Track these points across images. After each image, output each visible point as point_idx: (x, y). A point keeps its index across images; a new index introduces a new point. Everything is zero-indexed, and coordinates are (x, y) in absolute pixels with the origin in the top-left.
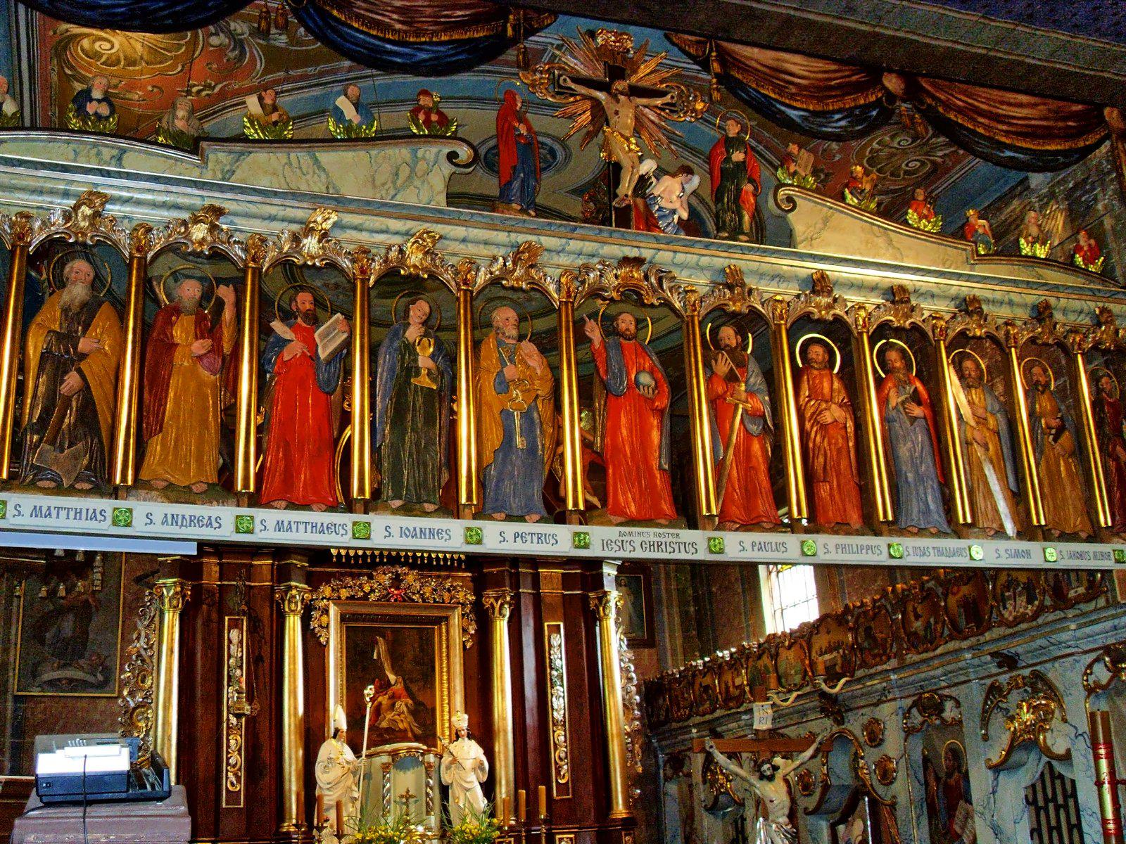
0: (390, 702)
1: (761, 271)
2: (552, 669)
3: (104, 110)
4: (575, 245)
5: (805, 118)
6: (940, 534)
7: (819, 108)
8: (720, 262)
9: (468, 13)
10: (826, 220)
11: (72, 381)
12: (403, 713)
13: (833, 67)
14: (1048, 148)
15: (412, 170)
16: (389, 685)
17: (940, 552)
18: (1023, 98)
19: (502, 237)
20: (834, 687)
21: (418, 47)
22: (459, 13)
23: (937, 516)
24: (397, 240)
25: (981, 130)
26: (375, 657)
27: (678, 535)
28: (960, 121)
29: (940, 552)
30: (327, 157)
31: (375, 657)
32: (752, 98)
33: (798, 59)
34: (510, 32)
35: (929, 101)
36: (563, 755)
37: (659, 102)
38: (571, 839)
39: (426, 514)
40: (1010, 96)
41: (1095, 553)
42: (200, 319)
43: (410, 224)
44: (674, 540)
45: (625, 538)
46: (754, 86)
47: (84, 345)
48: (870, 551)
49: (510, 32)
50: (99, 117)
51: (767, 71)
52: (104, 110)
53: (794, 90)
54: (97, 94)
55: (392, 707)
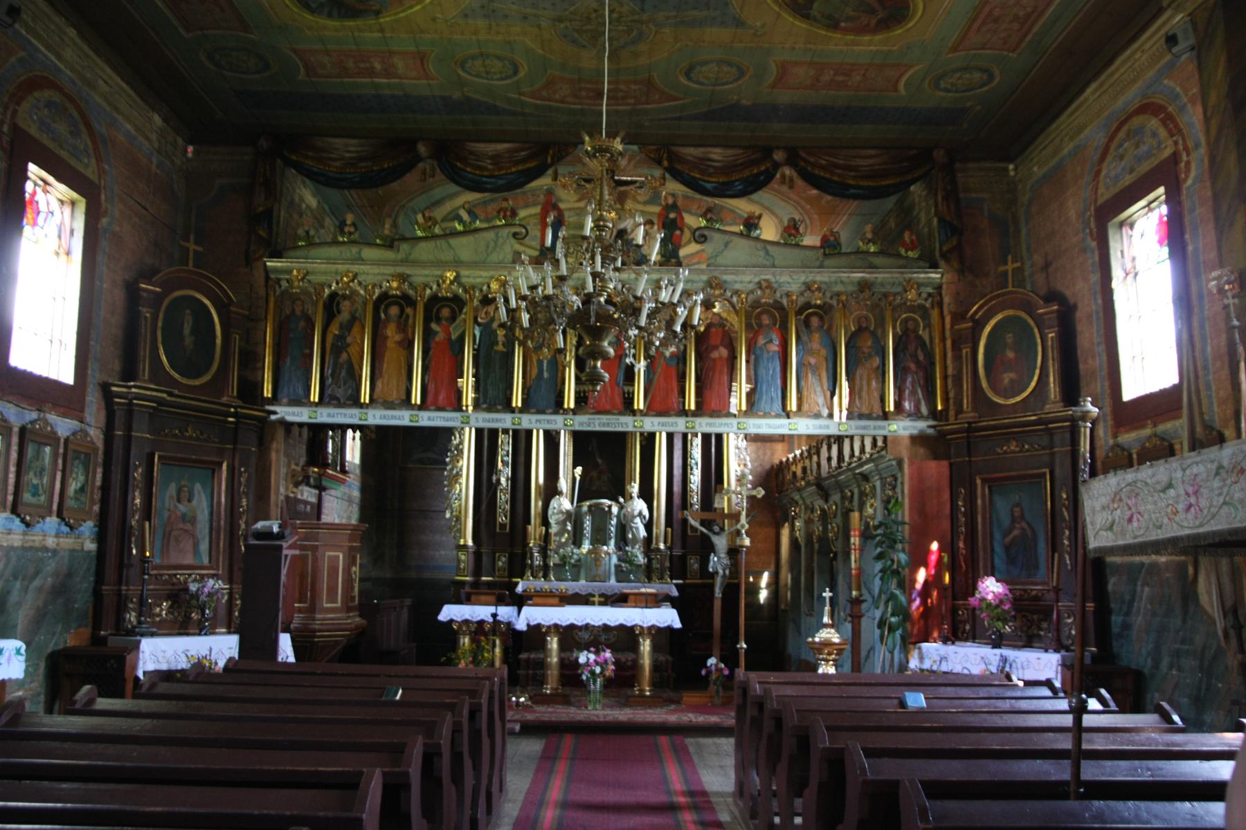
3: (352, 229)
5: (715, 188)
6: (778, 416)
10: (726, 245)
11: (344, 356)
14: (883, 183)
18: (872, 152)
20: (336, 602)
23: (777, 405)
25: (836, 178)
30: (454, 241)
33: (718, 150)
34: (549, 160)
35: (802, 164)
39: (498, 411)
43: (492, 273)
47: (349, 340)
49: (549, 160)
52: (352, 229)
53: (711, 170)
54: (349, 222)
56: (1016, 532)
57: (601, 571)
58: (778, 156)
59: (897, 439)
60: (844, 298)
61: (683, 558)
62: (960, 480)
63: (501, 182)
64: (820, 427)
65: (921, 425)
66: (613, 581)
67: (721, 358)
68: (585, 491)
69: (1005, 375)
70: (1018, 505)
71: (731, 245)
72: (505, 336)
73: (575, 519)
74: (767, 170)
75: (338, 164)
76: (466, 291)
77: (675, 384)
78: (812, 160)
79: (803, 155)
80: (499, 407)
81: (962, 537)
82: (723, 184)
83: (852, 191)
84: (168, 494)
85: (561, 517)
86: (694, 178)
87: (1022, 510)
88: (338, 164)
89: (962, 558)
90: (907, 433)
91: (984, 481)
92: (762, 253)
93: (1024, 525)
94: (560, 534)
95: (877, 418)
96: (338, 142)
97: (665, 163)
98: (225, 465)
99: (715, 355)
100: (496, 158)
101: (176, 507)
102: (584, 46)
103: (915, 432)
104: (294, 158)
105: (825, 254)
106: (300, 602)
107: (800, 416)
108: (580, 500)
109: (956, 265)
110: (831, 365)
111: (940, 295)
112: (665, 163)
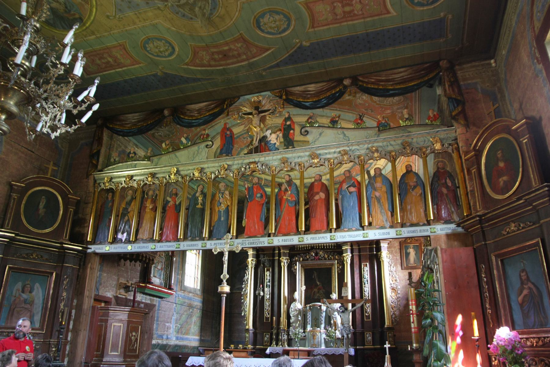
4: (236, 162)
6: (357, 230)
7: (317, 99)
8: (279, 157)
10: (320, 134)
13: (325, 84)
14: (410, 85)
15: (198, 152)
16: (317, 285)
17: (350, 236)
18: (402, 70)
19: (217, 165)
21: (200, 119)
23: (295, 229)
24: (192, 171)
25: (381, 87)
29: (350, 236)
33: (312, 85)
34: (225, 106)
35: (360, 83)
39: (196, 240)
40: (396, 71)
41: (340, 236)
42: (152, 199)
43: (194, 167)
49: (225, 106)
50: (132, 157)
52: (133, 155)
53: (309, 96)
54: (132, 152)
55: (318, 292)
56: (525, 292)
57: (316, 341)
58: (347, 82)
59: (437, 238)
60: (394, 154)
61: (363, 334)
62: (480, 258)
63: (201, 121)
64: (384, 234)
65: (451, 228)
66: (323, 347)
67: (321, 198)
68: (309, 299)
69: (500, 180)
70: (523, 270)
71: (323, 134)
72: (202, 200)
73: (303, 314)
74: (340, 90)
75: (129, 126)
76: (182, 178)
77: (294, 218)
78: (366, 80)
79: (361, 79)
80: (197, 238)
81: (488, 301)
82: (315, 102)
83: (391, 92)
84: (16, 288)
85: (296, 313)
86: (299, 101)
87: (527, 274)
88: (129, 126)
89: (490, 317)
90: (444, 232)
91: (497, 256)
92: (342, 136)
93: (530, 285)
94: (296, 322)
95: (424, 225)
96: (130, 116)
97: (284, 97)
98: (54, 274)
99: (317, 197)
100: (199, 111)
101: (20, 295)
102: (191, 18)
103: (449, 231)
104: (111, 126)
105: (379, 130)
106: (97, 351)
107: (371, 229)
108: (306, 303)
109: (462, 122)
110: (390, 197)
111: (457, 144)
112: (284, 97)
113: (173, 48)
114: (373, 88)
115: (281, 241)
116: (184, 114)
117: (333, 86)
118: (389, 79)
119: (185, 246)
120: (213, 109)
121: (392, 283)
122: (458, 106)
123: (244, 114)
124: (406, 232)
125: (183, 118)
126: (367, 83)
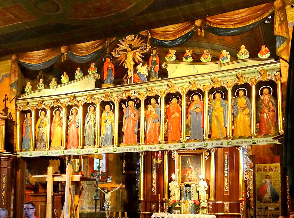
0: (191, 172)
1: (156, 85)
2: (225, 164)
9: (98, 44)
10: (177, 67)
12: (194, 175)
22: (97, 44)
25: (224, 27)
26: (188, 162)
27: (133, 147)
28: (217, 27)
31: (188, 162)
32: (158, 42)
35: (208, 24)
36: (227, 185)
37: (138, 50)
38: (211, 204)
41: (188, 145)
44: (132, 148)
45: (123, 149)
46: (158, 39)
48: (176, 147)
51: (162, 33)
74: (192, 30)
75: (36, 61)
99: (174, 116)
100: (87, 49)
113: (58, 7)
114: (218, 28)
115: (148, 148)
116: (76, 51)
117: (188, 26)
118: (231, 19)
119: (84, 151)
120: (97, 47)
121: (246, 167)
122: (283, 43)
123: (121, 51)
124: (234, 143)
125: (75, 55)
126: (214, 23)
